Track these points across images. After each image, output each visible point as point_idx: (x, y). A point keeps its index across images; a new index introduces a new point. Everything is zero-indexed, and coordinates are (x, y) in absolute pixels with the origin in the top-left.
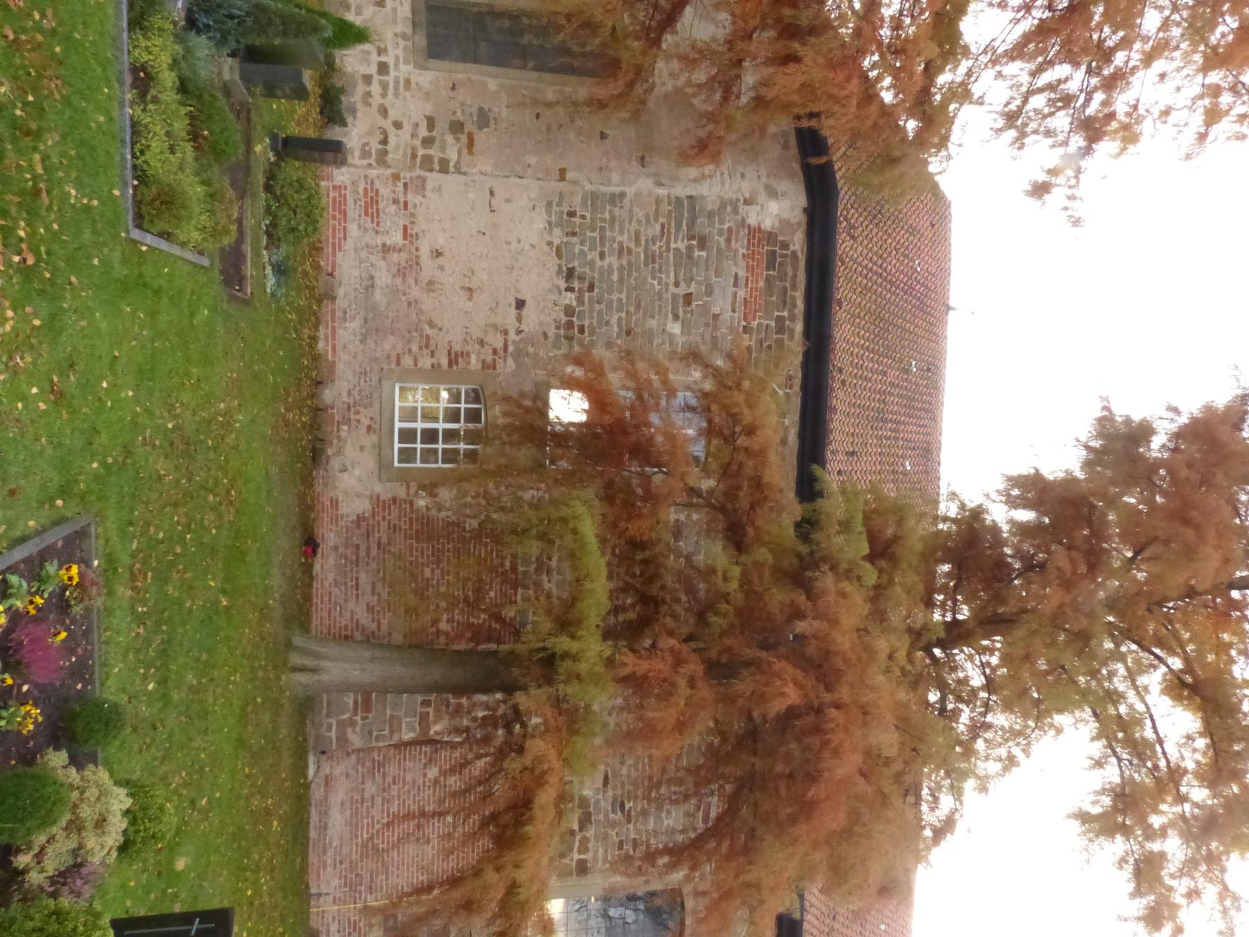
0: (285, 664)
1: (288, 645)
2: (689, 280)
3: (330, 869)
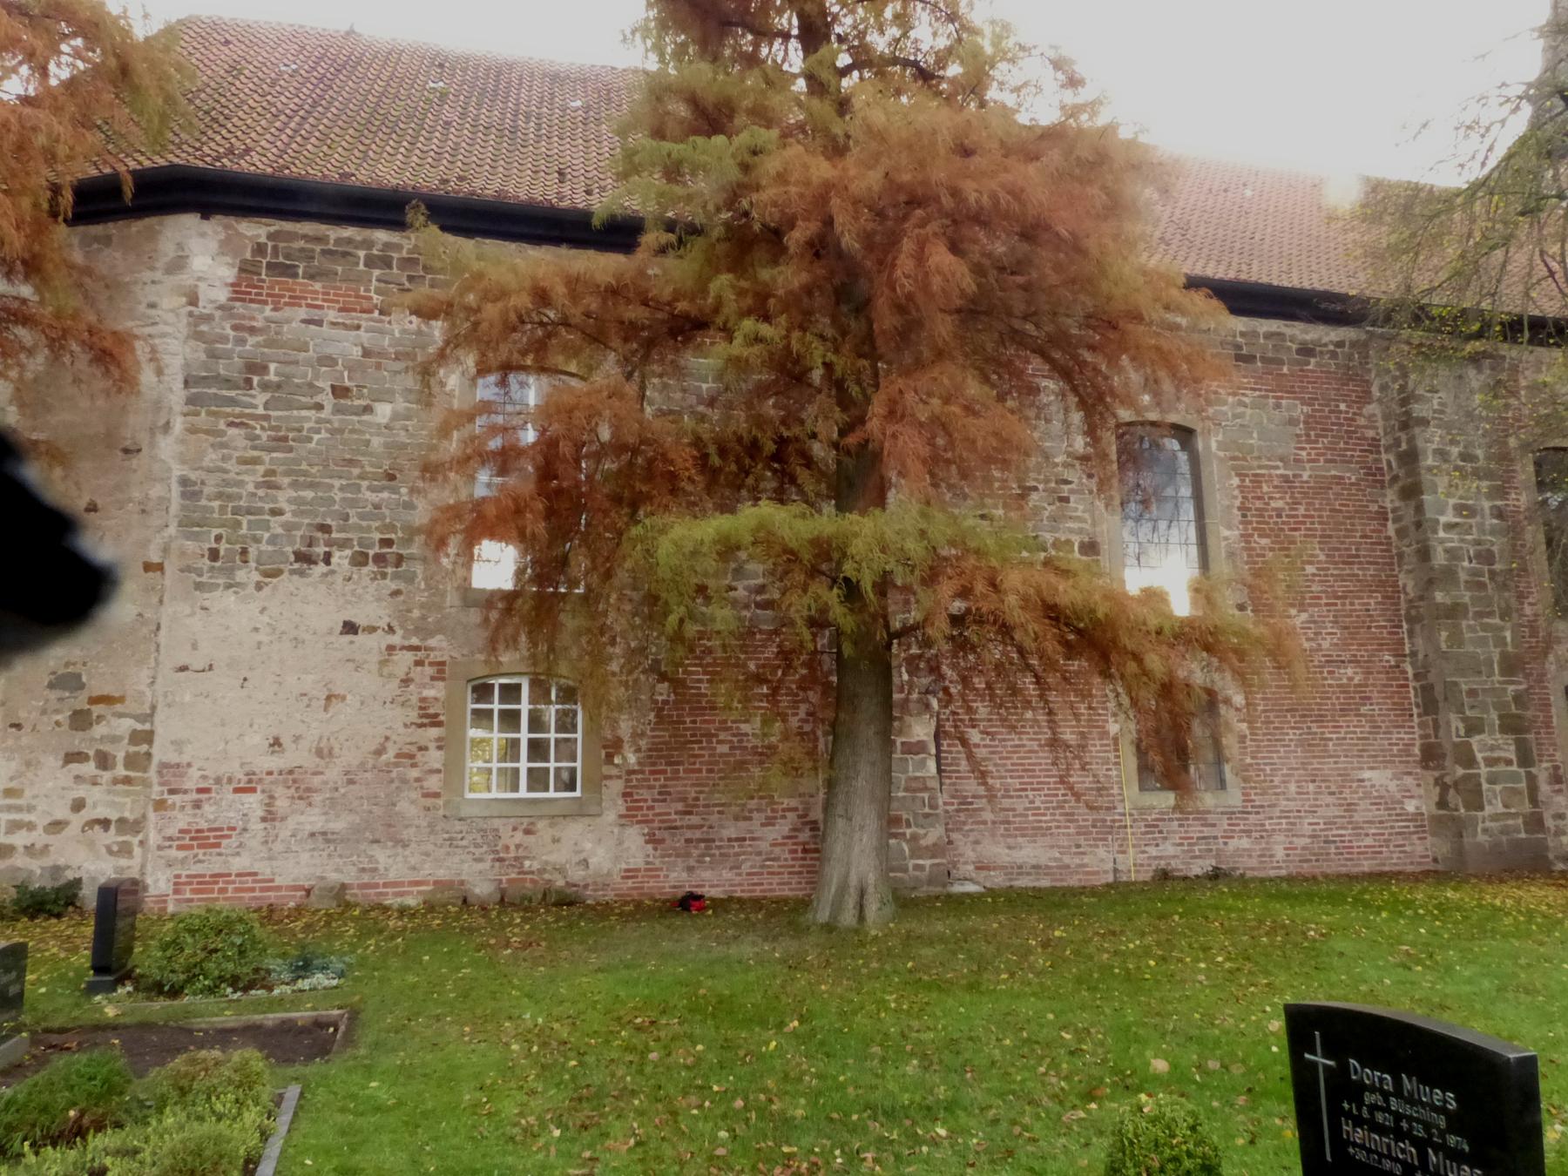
0: (856, 932)
1: (829, 928)
2: (312, 388)
3: (1086, 860)
